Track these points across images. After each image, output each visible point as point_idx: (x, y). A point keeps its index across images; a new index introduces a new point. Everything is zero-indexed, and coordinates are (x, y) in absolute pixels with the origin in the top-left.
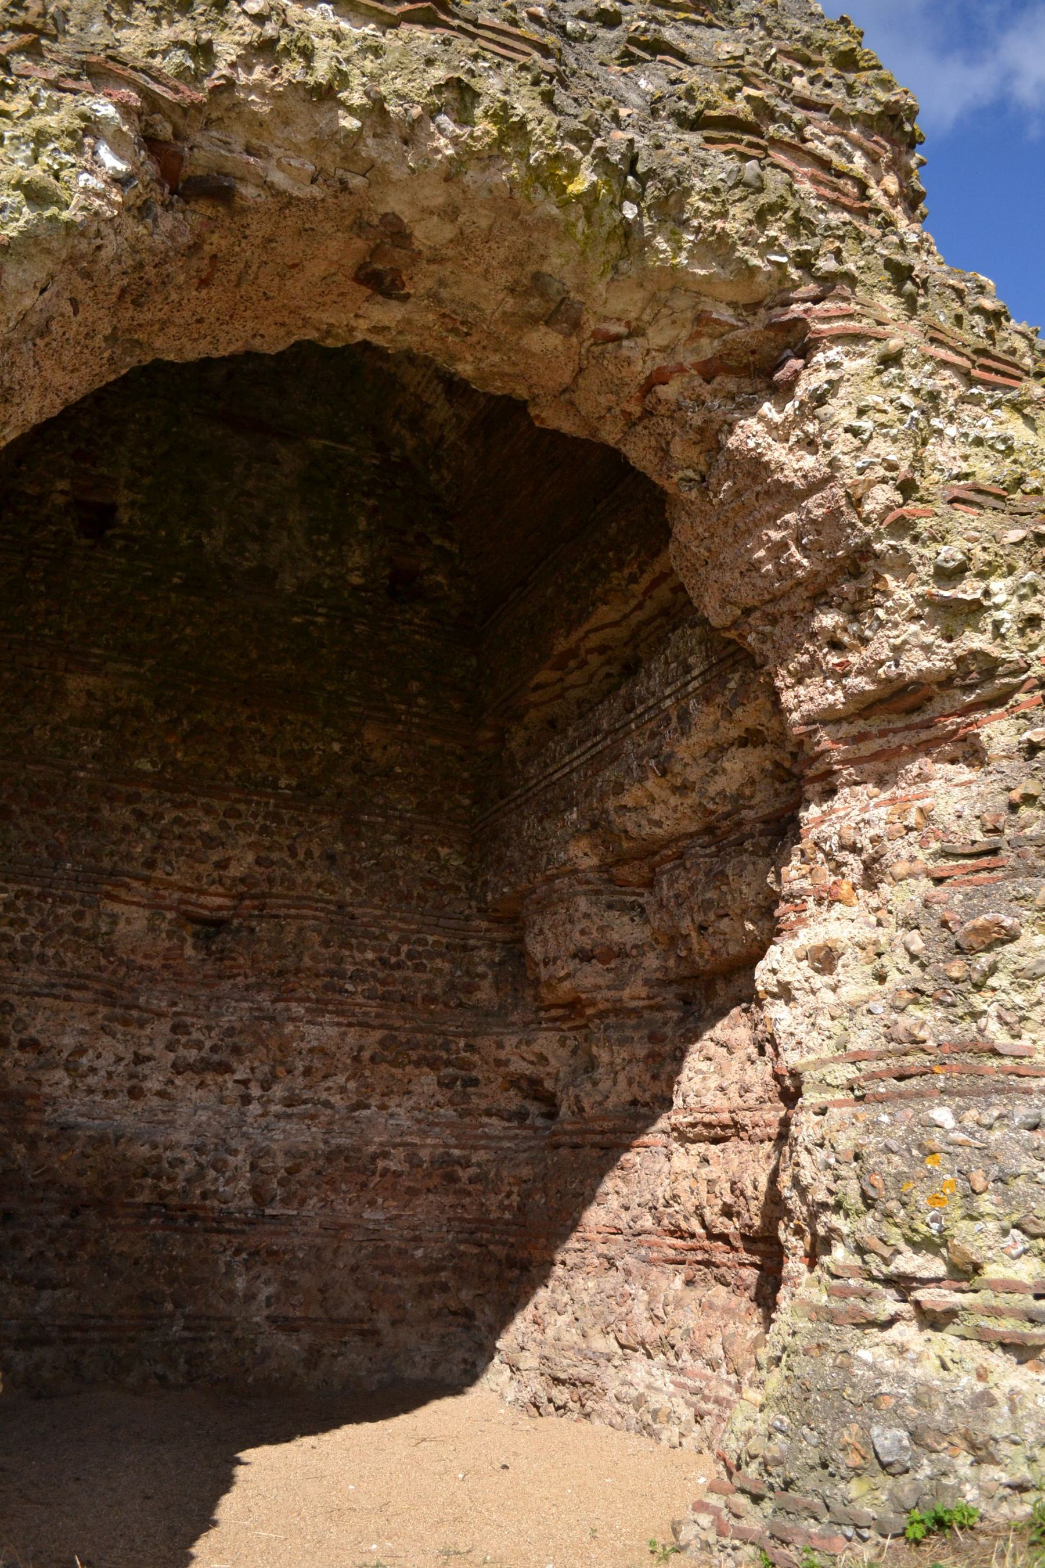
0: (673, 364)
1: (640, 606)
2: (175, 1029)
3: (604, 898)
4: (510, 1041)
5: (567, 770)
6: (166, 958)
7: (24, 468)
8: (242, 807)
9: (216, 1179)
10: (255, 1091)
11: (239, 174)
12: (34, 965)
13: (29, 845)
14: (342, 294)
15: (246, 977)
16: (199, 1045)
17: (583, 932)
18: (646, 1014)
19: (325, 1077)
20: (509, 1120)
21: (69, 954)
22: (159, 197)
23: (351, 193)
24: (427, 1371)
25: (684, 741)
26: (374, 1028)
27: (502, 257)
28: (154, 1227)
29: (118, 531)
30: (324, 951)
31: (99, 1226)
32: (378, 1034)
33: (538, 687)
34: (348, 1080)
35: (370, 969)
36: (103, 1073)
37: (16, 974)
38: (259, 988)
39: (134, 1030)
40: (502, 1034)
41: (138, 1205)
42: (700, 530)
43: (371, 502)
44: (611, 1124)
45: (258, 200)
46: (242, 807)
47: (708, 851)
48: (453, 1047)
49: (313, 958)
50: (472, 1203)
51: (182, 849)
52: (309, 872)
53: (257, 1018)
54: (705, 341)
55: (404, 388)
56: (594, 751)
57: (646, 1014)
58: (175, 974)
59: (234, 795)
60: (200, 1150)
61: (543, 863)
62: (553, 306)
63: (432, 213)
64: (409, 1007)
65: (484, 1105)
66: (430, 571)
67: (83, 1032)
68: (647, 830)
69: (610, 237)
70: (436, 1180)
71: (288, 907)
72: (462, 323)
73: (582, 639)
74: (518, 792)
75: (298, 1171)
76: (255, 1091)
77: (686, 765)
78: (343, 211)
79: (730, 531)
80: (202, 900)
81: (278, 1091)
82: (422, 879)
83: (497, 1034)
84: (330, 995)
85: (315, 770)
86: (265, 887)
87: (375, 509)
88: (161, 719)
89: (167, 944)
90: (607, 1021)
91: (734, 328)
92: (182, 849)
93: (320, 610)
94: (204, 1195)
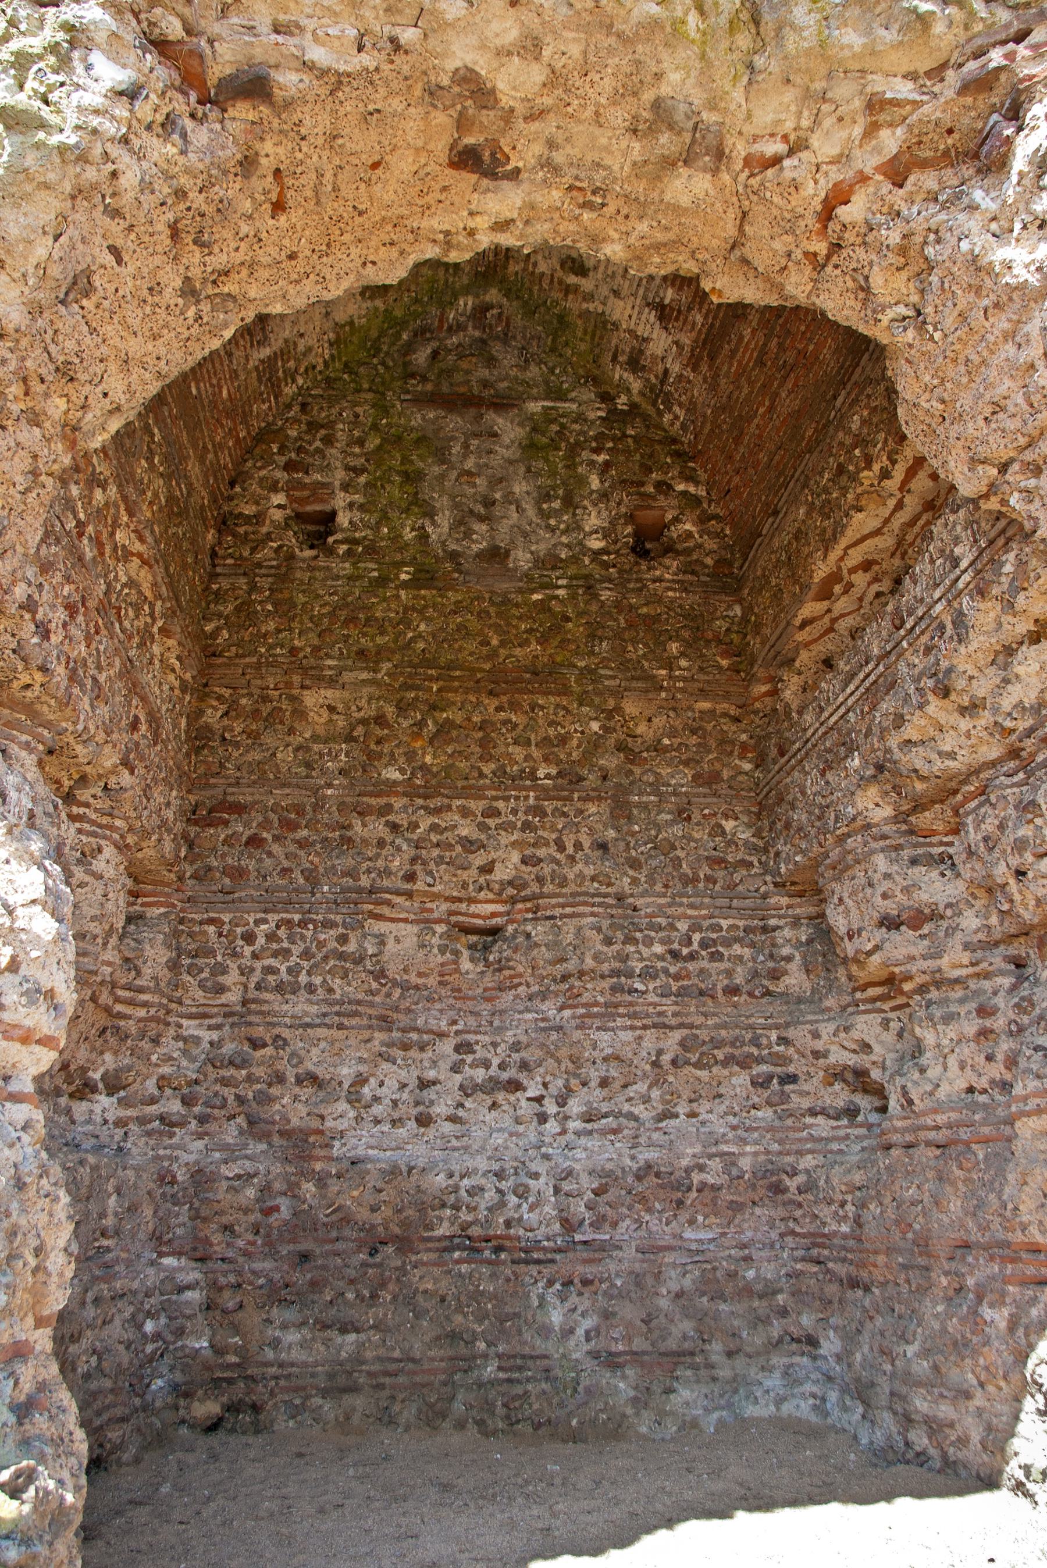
0: (851, 174)
1: (900, 506)
2: (457, 1049)
3: (906, 854)
4: (827, 1029)
5: (842, 710)
6: (442, 975)
7: (238, 489)
8: (500, 804)
9: (519, 1206)
10: (551, 1108)
11: (272, 62)
12: (303, 995)
13: (285, 871)
14: (445, 189)
15: (528, 986)
16: (486, 1064)
17: (885, 896)
18: (973, 984)
19: (625, 1086)
20: (837, 1118)
21: (338, 981)
22: (185, 107)
23: (406, 52)
24: (772, 1408)
25: (962, 650)
26: (671, 1028)
27: (609, 90)
28: (458, 1262)
29: (339, 536)
30: (605, 949)
31: (399, 1263)
32: (677, 1035)
33: (804, 624)
34: (650, 1087)
35: (660, 964)
36: (387, 1101)
37: (285, 1007)
38: (544, 996)
39: (414, 1053)
40: (817, 1021)
41: (439, 1239)
42: (927, 378)
43: (602, 458)
44: (945, 1117)
45: (301, 86)
46: (500, 804)
47: (1015, 779)
48: (764, 1041)
49: (595, 957)
50: (804, 1216)
51: (441, 857)
52: (580, 866)
53: (543, 1030)
54: (884, 133)
55: (616, 326)
56: (867, 683)
57: (973, 984)
58: (453, 990)
59: (490, 793)
60: (500, 1175)
61: (831, 823)
62: (687, 137)
63: (509, 54)
64: (710, 1002)
65: (806, 1103)
66: (676, 520)
67: (361, 1060)
68: (938, 764)
69: (733, 26)
70: (762, 1192)
71: (563, 906)
72: (594, 193)
73: (841, 559)
74: (797, 745)
75: (606, 1191)
76: (551, 1108)
77: (971, 678)
78: (406, 79)
79: (962, 369)
80: (473, 908)
81: (575, 1107)
82: (707, 858)
83: (811, 1022)
84: (619, 997)
85: (575, 755)
86: (535, 888)
87: (607, 465)
88: (405, 724)
89: (440, 959)
90: (928, 996)
91: (916, 104)
92: (441, 857)
93: (560, 582)
94: (508, 1224)
